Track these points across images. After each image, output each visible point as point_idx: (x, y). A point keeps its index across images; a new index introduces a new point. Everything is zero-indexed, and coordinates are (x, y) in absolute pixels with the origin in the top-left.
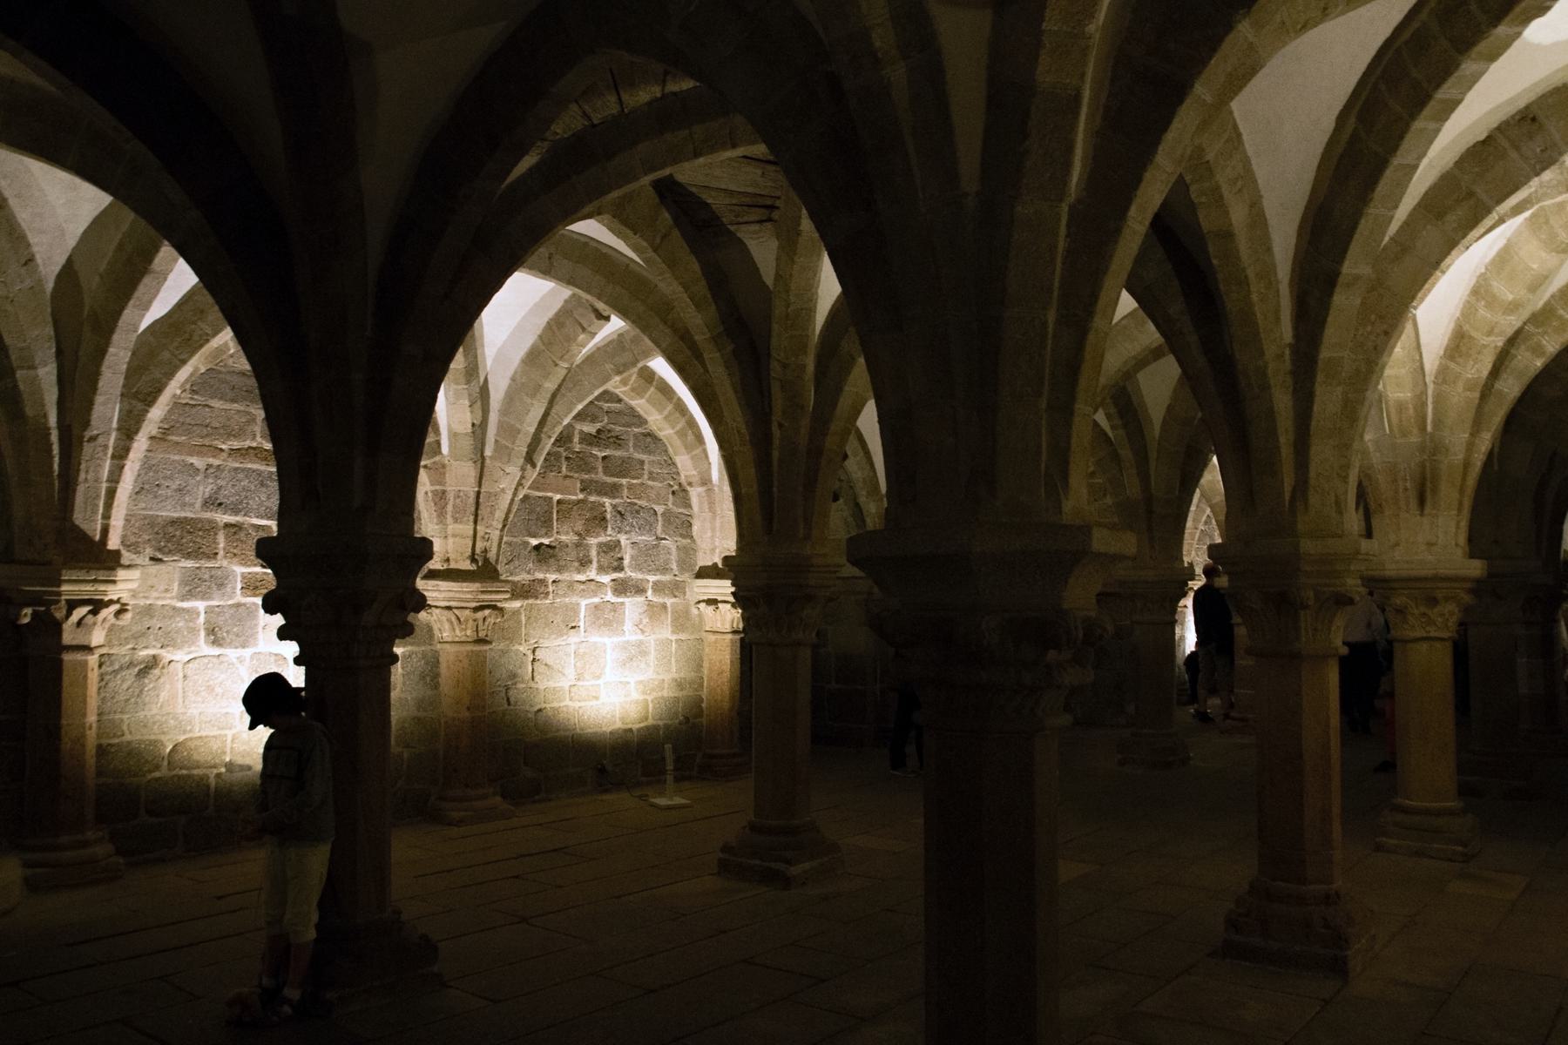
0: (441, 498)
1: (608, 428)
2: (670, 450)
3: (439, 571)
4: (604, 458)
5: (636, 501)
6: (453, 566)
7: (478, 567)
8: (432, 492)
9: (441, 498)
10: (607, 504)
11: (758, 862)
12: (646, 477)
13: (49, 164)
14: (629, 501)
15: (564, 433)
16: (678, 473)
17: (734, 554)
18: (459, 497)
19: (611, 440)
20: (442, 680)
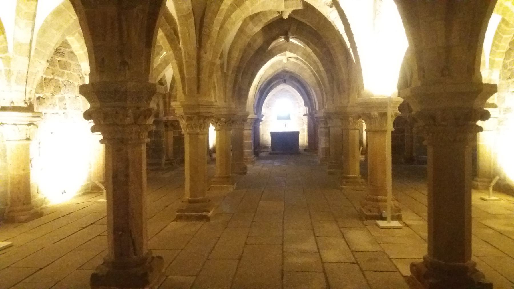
0: (9, 73)
1: (60, 48)
2: (79, 60)
3: (8, 107)
4: (59, 61)
5: (69, 80)
6: (16, 104)
7: (28, 105)
8: (5, 70)
9: (9, 73)
10: (60, 81)
11: (196, 213)
12: (72, 70)
13: (167, 8)
14: (67, 80)
15: (506, 79)
16: (81, 70)
17: (184, 100)
18: (19, 73)
19: (61, 53)
20: (8, 158)
